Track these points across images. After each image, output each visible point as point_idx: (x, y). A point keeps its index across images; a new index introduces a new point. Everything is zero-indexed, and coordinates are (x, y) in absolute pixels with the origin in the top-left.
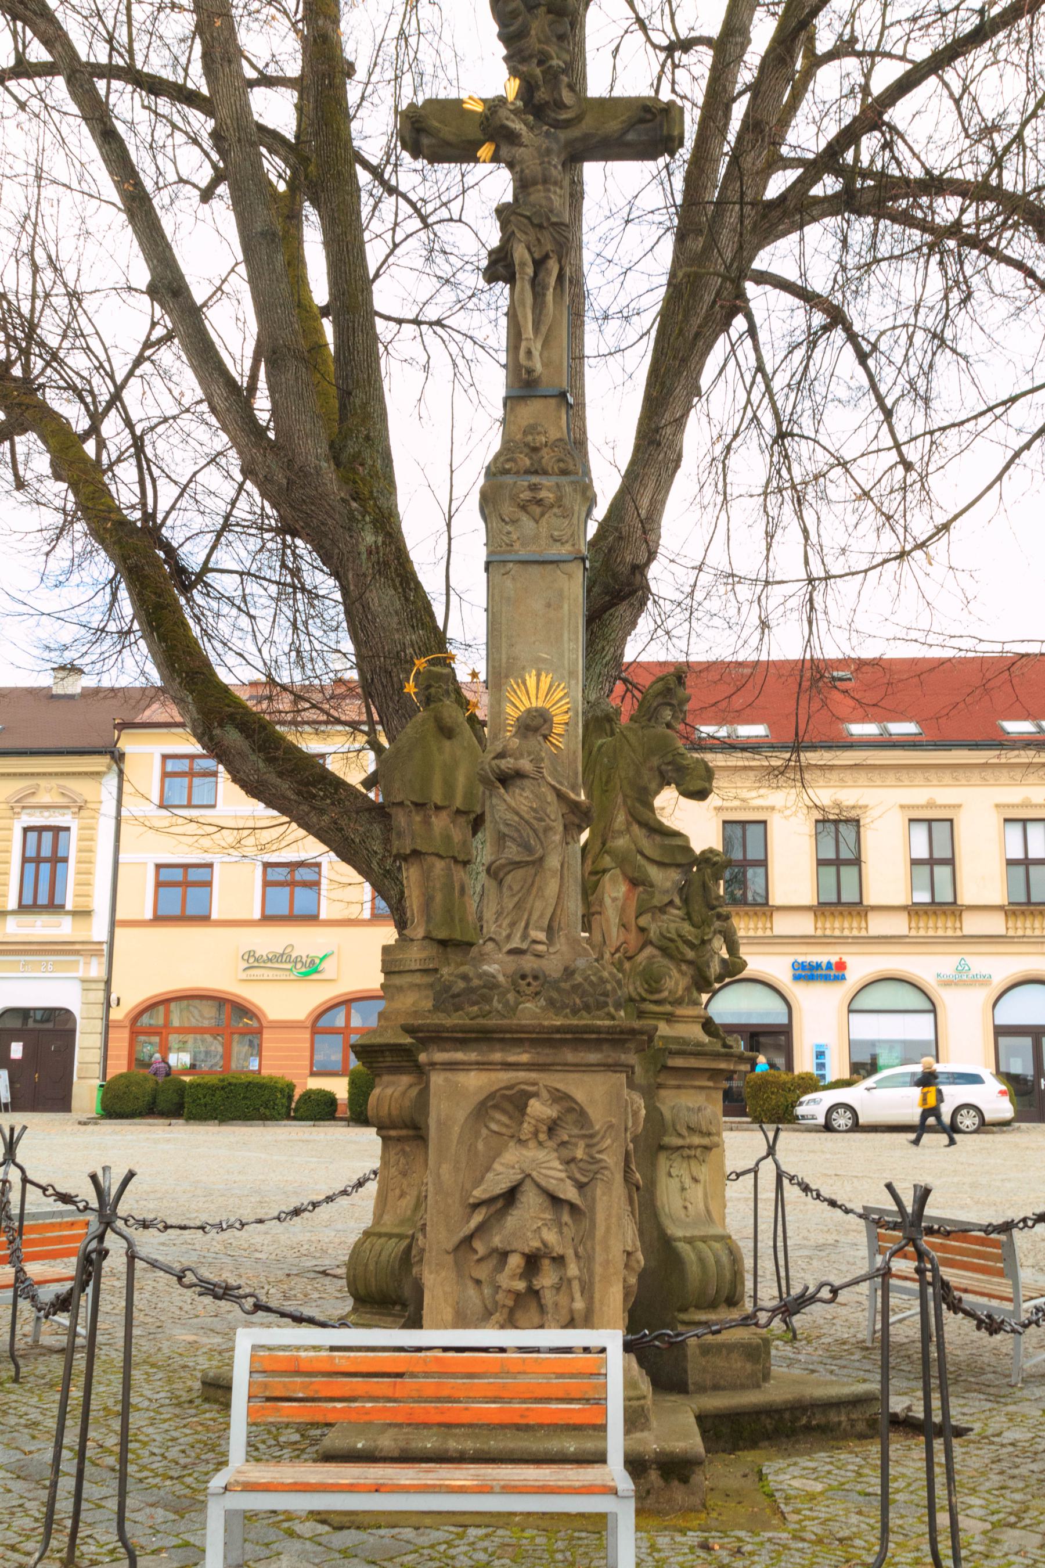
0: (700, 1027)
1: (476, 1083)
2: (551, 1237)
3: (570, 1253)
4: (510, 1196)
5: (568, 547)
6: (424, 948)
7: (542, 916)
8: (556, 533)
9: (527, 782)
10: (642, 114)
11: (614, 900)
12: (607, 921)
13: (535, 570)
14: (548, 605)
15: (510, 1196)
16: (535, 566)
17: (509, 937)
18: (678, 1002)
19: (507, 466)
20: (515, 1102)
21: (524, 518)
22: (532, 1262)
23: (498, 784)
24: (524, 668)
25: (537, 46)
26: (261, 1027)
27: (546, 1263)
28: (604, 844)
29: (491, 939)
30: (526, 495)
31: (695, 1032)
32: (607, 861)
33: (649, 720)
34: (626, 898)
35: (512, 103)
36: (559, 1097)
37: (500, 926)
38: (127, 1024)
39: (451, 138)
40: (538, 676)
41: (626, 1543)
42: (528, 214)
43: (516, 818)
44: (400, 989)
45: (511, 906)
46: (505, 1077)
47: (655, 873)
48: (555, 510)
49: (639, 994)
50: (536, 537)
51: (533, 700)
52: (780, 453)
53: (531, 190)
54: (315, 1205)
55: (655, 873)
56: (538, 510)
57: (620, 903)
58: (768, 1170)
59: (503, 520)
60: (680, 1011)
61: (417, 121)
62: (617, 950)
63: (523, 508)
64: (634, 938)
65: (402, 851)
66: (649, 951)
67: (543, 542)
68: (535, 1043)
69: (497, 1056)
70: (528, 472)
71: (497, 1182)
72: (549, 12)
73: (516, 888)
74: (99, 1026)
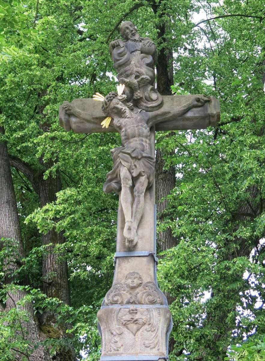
5: (155, 351)
8: (147, 342)
10: (196, 103)
19: (115, 299)
21: (125, 330)
25: (135, 69)
30: (128, 317)
35: (120, 96)
39: (87, 117)
42: (129, 152)
48: (146, 327)
50: (133, 346)
52: (57, 212)
53: (131, 140)
56: (134, 327)
59: (112, 334)
61: (69, 110)
63: (125, 325)
67: (138, 349)
70: (129, 303)
72: (142, 53)
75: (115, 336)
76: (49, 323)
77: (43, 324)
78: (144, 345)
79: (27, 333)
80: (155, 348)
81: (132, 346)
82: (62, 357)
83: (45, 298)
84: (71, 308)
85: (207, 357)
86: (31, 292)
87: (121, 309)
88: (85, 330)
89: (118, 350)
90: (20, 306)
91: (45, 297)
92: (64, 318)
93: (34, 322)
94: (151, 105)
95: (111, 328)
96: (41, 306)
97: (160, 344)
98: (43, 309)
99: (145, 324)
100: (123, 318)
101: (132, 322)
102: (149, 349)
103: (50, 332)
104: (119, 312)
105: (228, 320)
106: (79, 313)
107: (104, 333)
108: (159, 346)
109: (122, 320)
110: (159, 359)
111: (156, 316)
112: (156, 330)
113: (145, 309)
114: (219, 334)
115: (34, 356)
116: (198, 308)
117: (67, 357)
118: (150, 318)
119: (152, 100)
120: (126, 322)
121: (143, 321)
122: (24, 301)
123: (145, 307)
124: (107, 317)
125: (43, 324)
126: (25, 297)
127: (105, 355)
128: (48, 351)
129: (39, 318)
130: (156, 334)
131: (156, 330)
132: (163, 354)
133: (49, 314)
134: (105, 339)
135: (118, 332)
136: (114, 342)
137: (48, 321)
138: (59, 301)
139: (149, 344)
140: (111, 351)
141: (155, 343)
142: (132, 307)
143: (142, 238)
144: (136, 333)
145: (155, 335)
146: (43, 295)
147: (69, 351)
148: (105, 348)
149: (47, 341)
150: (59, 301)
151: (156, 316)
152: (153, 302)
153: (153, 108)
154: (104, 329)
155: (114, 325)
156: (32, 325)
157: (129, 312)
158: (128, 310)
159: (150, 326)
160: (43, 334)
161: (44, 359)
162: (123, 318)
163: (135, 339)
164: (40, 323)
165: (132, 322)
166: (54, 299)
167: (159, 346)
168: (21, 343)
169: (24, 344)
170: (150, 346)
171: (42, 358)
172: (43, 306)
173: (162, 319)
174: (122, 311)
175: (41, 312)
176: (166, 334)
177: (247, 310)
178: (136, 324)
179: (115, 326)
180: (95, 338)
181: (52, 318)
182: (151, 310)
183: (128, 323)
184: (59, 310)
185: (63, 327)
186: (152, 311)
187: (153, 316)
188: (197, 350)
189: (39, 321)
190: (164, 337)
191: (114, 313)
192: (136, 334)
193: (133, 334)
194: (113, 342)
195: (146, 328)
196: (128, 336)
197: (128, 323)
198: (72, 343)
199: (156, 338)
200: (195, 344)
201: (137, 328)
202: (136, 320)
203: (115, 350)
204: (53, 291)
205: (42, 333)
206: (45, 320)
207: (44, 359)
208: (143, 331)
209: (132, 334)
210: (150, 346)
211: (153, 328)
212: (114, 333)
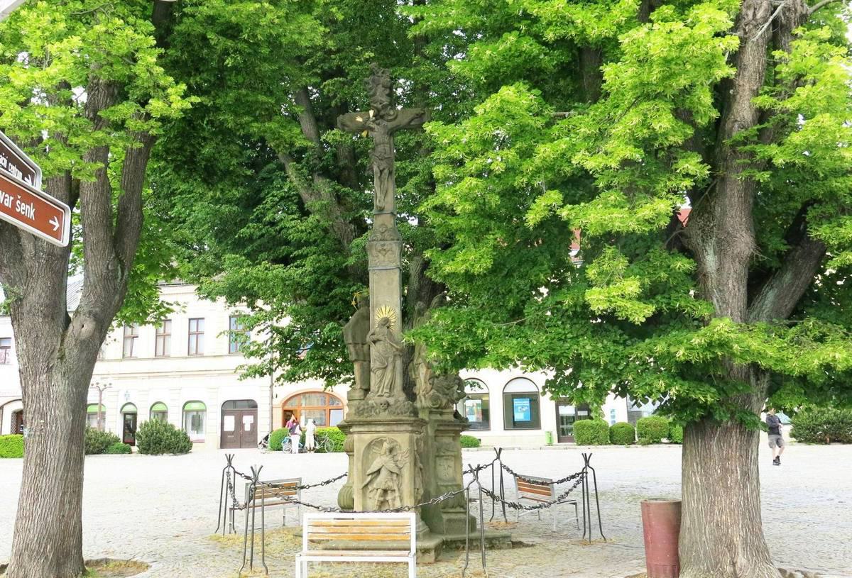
1: (368, 437)
2: (390, 484)
3: (396, 488)
4: (379, 471)
14: (389, 284)
15: (379, 471)
18: (445, 408)
20: (381, 442)
22: (385, 491)
27: (389, 492)
31: (451, 418)
34: (426, 373)
36: (392, 441)
38: (281, 406)
41: (412, 570)
46: (376, 436)
54: (335, 480)
58: (497, 464)
60: (444, 411)
64: (429, 387)
66: (433, 391)
68: (384, 424)
69: (373, 429)
71: (374, 468)
74: (268, 408)
94: (390, 118)
119: (390, 115)
123: (389, 242)
142: (382, 243)
143: (387, 203)
152: (393, 240)
153: (391, 120)
177: (796, 37)
179: (374, 252)
196: (381, 257)
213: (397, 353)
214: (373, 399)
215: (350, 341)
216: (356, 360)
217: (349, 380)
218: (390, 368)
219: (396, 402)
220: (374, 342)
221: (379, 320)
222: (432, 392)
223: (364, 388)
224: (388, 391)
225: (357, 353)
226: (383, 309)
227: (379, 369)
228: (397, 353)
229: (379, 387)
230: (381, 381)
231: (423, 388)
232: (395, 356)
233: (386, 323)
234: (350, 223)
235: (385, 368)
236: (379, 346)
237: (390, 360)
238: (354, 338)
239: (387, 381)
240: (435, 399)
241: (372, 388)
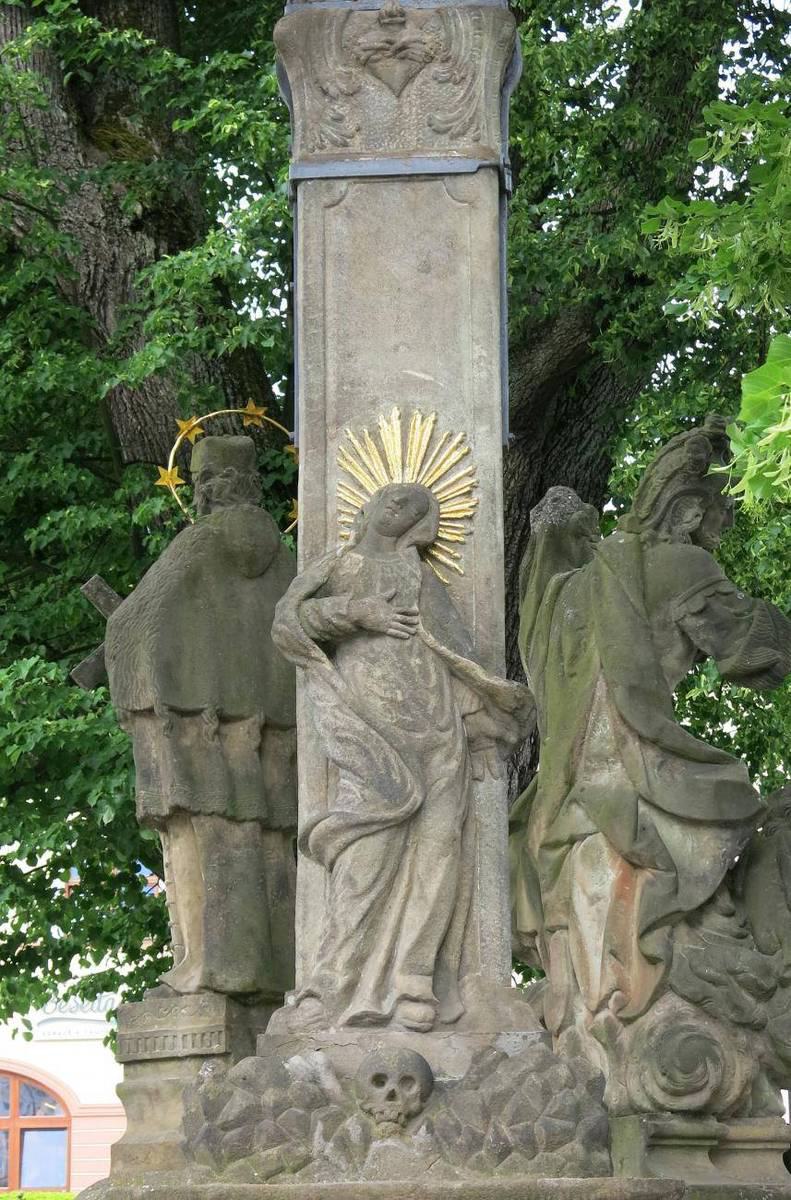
0: (779, 1160)
5: (465, 143)
6: (201, 1011)
7: (420, 942)
9: (378, 644)
11: (594, 899)
12: (580, 943)
13: (394, 194)
14: (426, 268)
16: (397, 186)
17: (351, 988)
18: (736, 1112)
21: (371, 86)
23: (318, 653)
24: (374, 403)
26: (69, 1118)
28: (570, 783)
29: (310, 995)
30: (375, 38)
32: (577, 818)
33: (657, 527)
34: (621, 893)
37: (331, 965)
40: (405, 419)
43: (360, 725)
44: (154, 1095)
45: (354, 920)
47: (673, 835)
48: (436, 68)
49: (654, 1103)
50: (394, 128)
51: (396, 469)
55: (673, 835)
56: (398, 69)
57: (605, 905)
59: (325, 93)
60: (736, 1130)
62: (602, 1005)
63: (366, 64)
64: (639, 978)
65: (153, 811)
66: (670, 1003)
67: (411, 138)
73: (362, 881)
75: (333, 99)
76: (114, 117)
77: (95, 120)
78: (430, 125)
79: (44, 145)
80: (463, 134)
81: (390, 130)
82: (162, 222)
83: (94, 33)
84: (181, 62)
85: (628, 204)
86: (50, 10)
87: (351, 11)
88: (235, 120)
89: (345, 145)
90: (14, 59)
91: (96, 27)
92: (160, 94)
93: (64, 115)
95: (321, 75)
96: (84, 56)
97: (483, 123)
98: (93, 68)
99: (432, 58)
100: (360, 40)
101: (389, 53)
102: (445, 138)
103: (120, 146)
104: (345, 22)
105: (694, 86)
106: (208, 77)
107: (300, 93)
108: (477, 129)
109: (356, 48)
110: (480, 168)
111: (467, 33)
112: (469, 78)
113: (432, 12)
114: (665, 135)
115: (70, 222)
116: (601, 49)
117: (178, 223)
118: (449, 41)
120: (369, 53)
121: (427, 48)
122: (28, 42)
124: (308, 38)
125: (95, 120)
126: (29, 29)
127: (304, 159)
128: (116, 206)
129: (77, 95)
130: (469, 89)
131: (469, 78)
132: (492, 153)
133: (112, 90)
134: (303, 109)
135: (343, 87)
136: (334, 119)
137: (110, 110)
138: (144, 38)
139: (447, 122)
140: (322, 148)
141: (467, 117)
144: (403, 89)
145: (465, 95)
146: (91, 21)
147: (183, 204)
148: (303, 137)
149: (109, 167)
150: (144, 38)
151: (467, 33)
154: (299, 78)
155: (331, 66)
156: (57, 124)
157: (379, 20)
158: (374, 14)
159: (450, 63)
160: (97, 151)
161: (105, 229)
162: (360, 40)
163: (400, 107)
164: (85, 117)
165: (389, 53)
166: (127, 34)
167: (477, 129)
168: (28, 177)
169: (38, 179)
170: (449, 129)
171: (99, 227)
172: (89, 58)
173: (488, 43)
174: (356, 18)
175: (87, 77)
176: (501, 91)
178: (403, 58)
179: (334, 69)
180: (266, 146)
181: (121, 101)
182: (450, 14)
183: (375, 57)
184: (143, 69)
185: (159, 128)
186: (455, 15)
187: (457, 34)
188: (592, 184)
189: (82, 112)
190: (495, 100)
191: (330, 25)
192: (405, 93)
193: (394, 92)
194: (328, 118)
195: (437, 72)
196: (377, 98)
197: (375, 57)
198: (190, 176)
199: (468, 104)
200: (587, 163)
201: (406, 72)
202: (403, 48)
203: (334, 143)
204: (122, 13)
205: (92, 148)
206: (98, 109)
207: (105, 229)
208: (425, 83)
209: (389, 92)
210: (449, 129)
211: (459, 72)
212: (333, 90)
213: (490, 725)
214: (312, 1044)
215: (148, 697)
216: (179, 814)
217: (108, 982)
218: (438, 824)
219: (485, 1064)
220: (332, 643)
221: (360, 501)
222: (659, 1012)
223: (234, 982)
224: (420, 985)
225: (188, 775)
226: (391, 434)
227: (365, 828)
228: (490, 725)
229: (358, 962)
230: (370, 921)
231: (598, 989)
232: (470, 743)
233: (408, 518)
234: (137, 225)
235: (411, 820)
236: (367, 673)
237: (444, 767)
238: (168, 674)
239: (412, 918)
240: (682, 1058)
241: (308, 967)
